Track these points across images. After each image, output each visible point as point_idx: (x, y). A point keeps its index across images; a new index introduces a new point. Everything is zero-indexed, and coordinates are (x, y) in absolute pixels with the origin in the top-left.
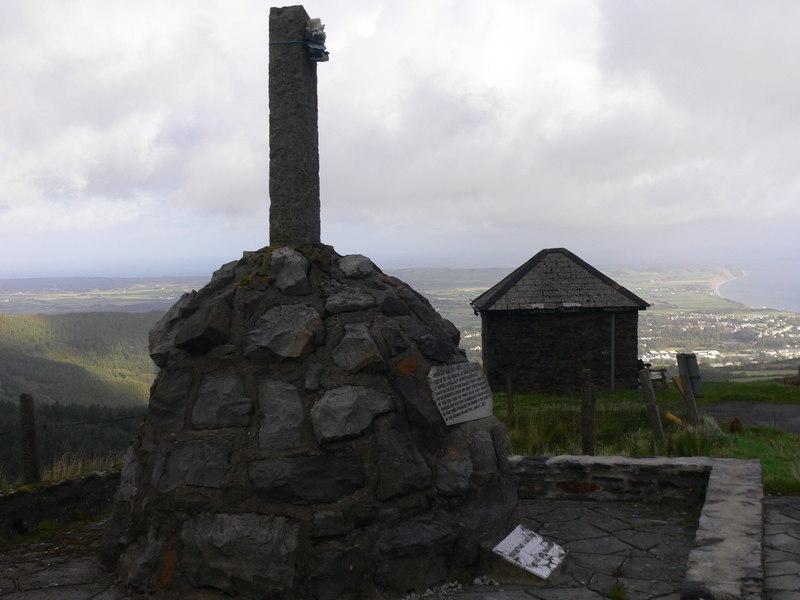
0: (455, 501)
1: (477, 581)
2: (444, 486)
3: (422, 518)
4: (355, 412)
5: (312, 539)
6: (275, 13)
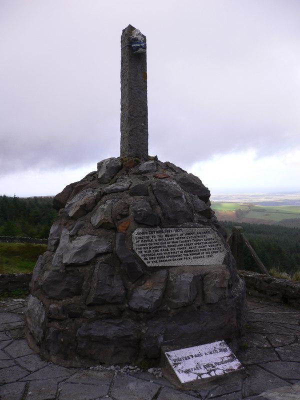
0: (142, 315)
1: (151, 370)
2: (134, 304)
3: (112, 321)
4: (85, 249)
5: (49, 318)
6: (130, 25)
